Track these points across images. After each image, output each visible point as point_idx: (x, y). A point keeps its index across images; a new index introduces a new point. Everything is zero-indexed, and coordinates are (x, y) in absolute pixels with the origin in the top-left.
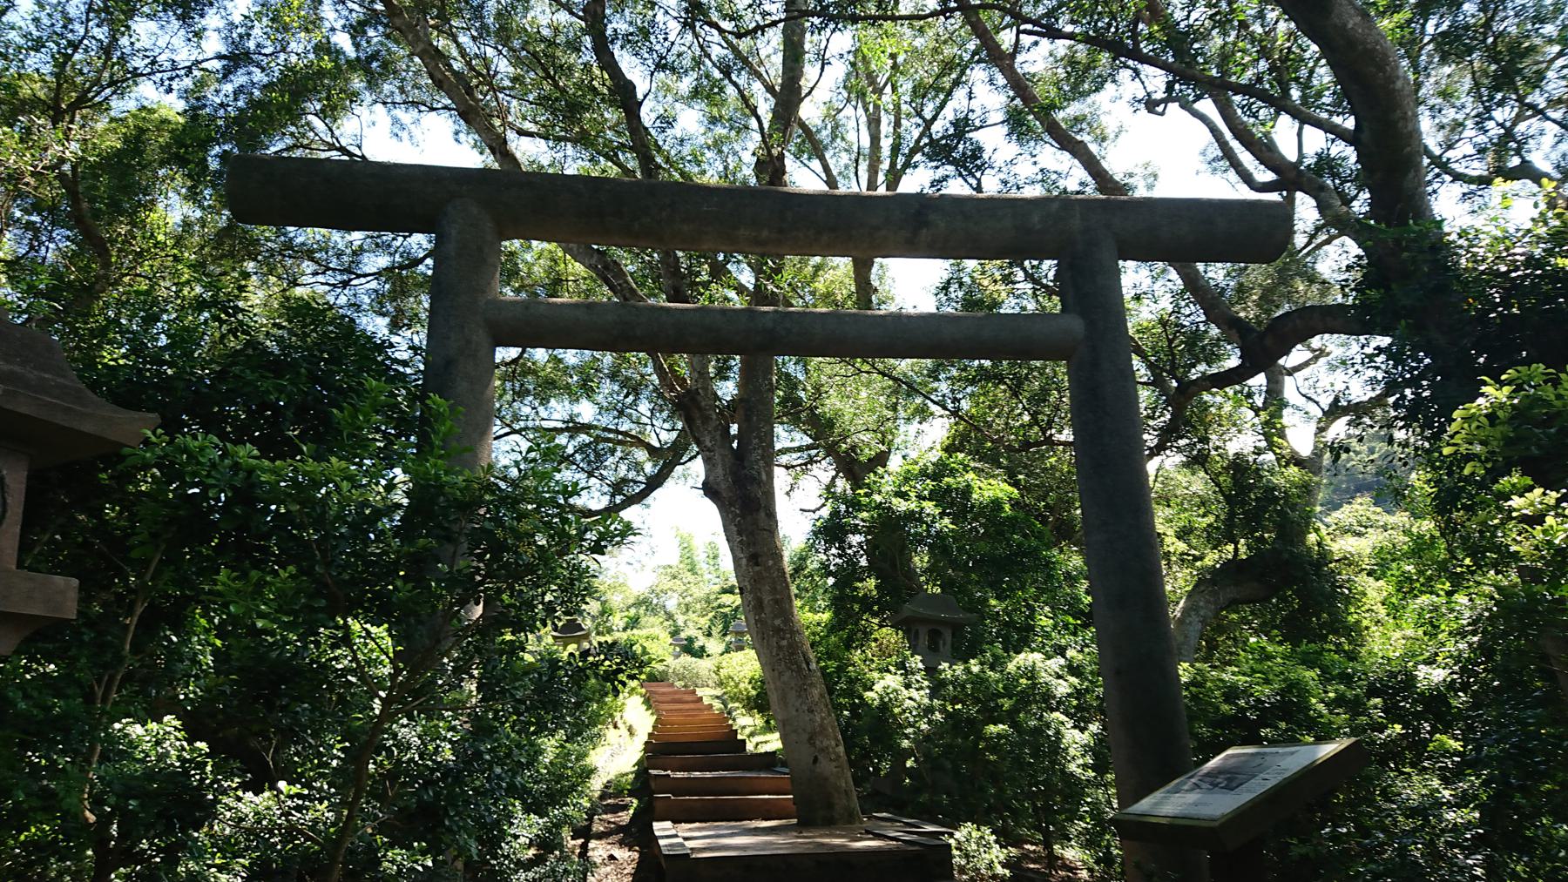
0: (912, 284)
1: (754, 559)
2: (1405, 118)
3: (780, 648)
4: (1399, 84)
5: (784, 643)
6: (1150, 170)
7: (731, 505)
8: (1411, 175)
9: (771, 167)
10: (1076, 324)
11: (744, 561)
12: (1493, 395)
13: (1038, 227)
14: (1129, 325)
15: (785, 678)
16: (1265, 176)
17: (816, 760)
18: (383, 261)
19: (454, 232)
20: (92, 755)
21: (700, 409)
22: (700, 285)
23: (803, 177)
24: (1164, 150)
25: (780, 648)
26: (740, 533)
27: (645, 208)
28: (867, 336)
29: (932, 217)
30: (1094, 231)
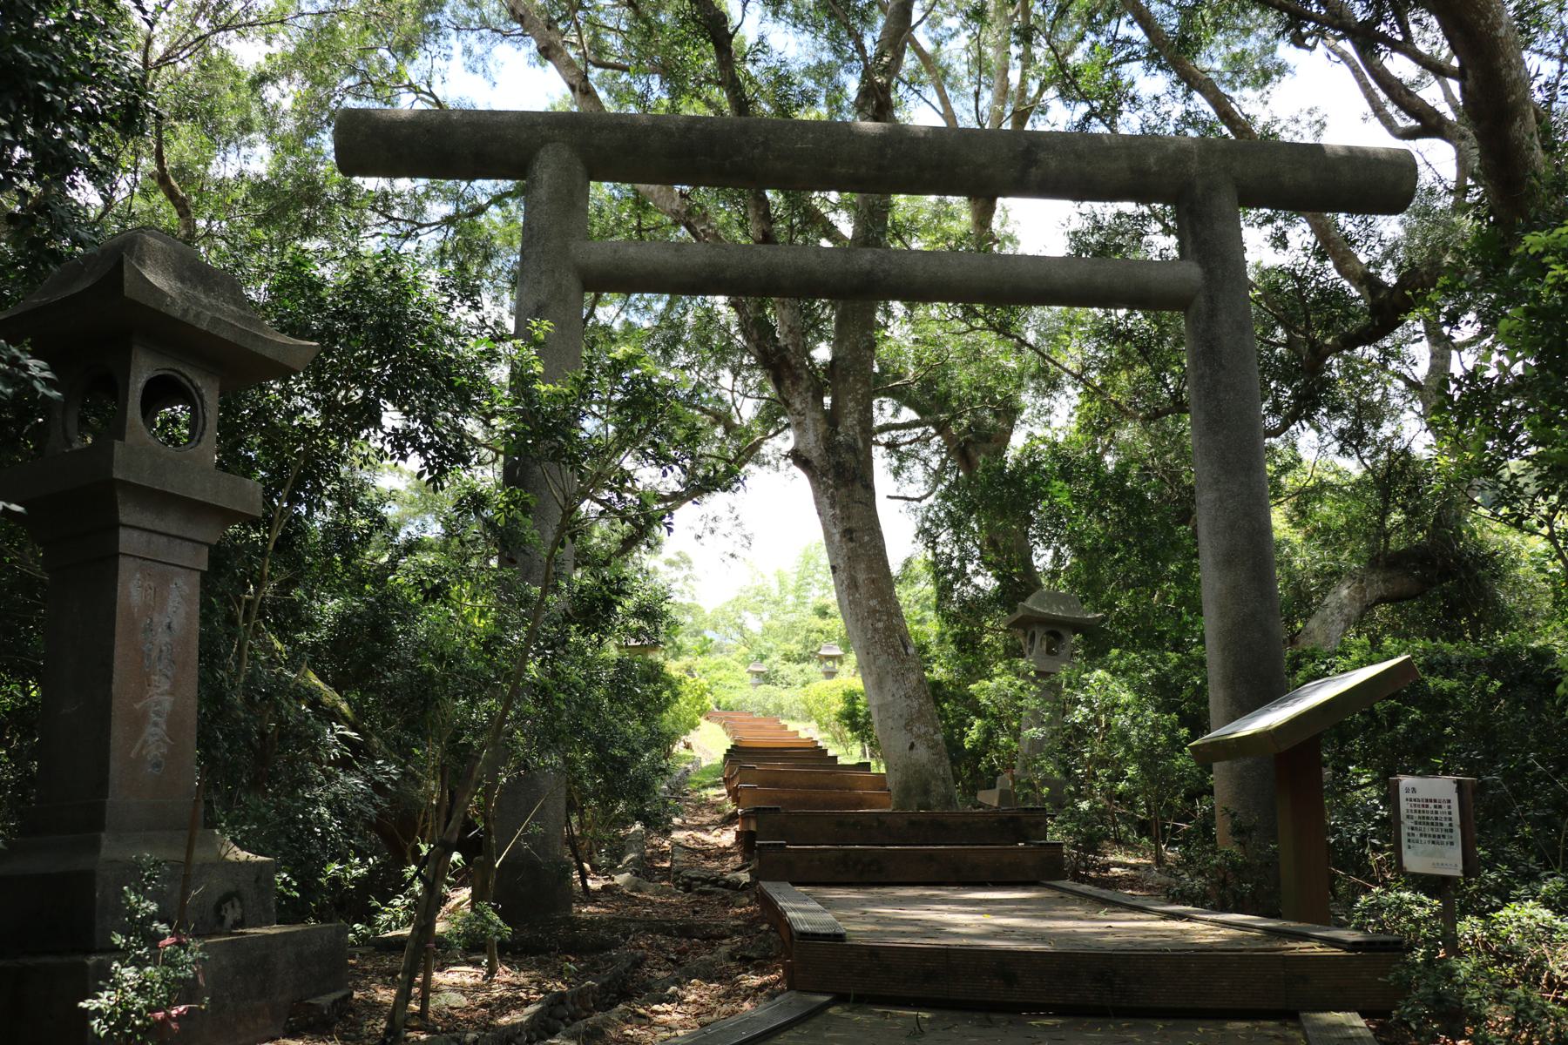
0: (1039, 227)
1: (848, 534)
2: (1509, 66)
3: (876, 630)
4: (1502, 32)
5: (880, 625)
6: (1316, 117)
7: (824, 474)
8: (1518, 123)
9: (877, 100)
10: (1193, 271)
11: (837, 537)
12: (1355, 293)
13: (1155, 169)
14: (654, 188)
15: (880, 662)
16: (1404, 122)
17: (912, 747)
18: (448, 209)
19: (545, 176)
20: (1365, 879)
21: (789, 367)
22: (767, 229)
23: (919, 112)
24: (1316, 97)
25: (876, 630)
26: (832, 506)
27: (749, 151)
28: (999, 288)
29: (1042, 155)
30: (1227, 174)
